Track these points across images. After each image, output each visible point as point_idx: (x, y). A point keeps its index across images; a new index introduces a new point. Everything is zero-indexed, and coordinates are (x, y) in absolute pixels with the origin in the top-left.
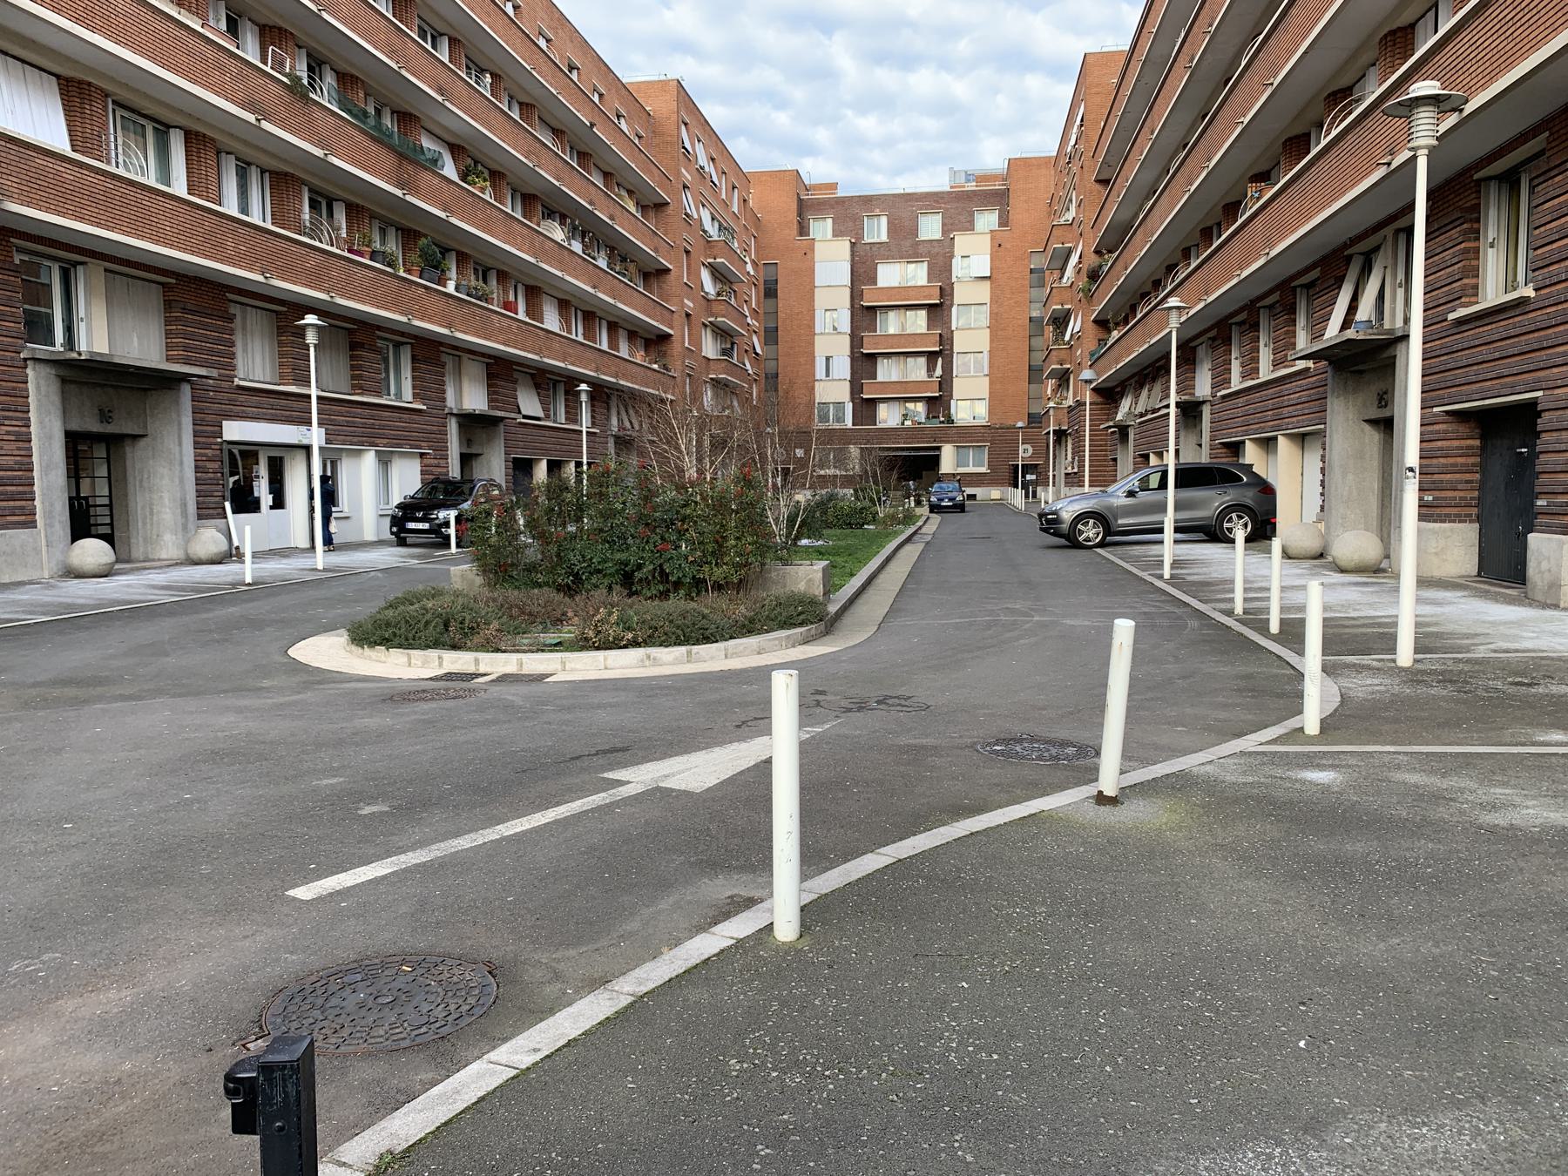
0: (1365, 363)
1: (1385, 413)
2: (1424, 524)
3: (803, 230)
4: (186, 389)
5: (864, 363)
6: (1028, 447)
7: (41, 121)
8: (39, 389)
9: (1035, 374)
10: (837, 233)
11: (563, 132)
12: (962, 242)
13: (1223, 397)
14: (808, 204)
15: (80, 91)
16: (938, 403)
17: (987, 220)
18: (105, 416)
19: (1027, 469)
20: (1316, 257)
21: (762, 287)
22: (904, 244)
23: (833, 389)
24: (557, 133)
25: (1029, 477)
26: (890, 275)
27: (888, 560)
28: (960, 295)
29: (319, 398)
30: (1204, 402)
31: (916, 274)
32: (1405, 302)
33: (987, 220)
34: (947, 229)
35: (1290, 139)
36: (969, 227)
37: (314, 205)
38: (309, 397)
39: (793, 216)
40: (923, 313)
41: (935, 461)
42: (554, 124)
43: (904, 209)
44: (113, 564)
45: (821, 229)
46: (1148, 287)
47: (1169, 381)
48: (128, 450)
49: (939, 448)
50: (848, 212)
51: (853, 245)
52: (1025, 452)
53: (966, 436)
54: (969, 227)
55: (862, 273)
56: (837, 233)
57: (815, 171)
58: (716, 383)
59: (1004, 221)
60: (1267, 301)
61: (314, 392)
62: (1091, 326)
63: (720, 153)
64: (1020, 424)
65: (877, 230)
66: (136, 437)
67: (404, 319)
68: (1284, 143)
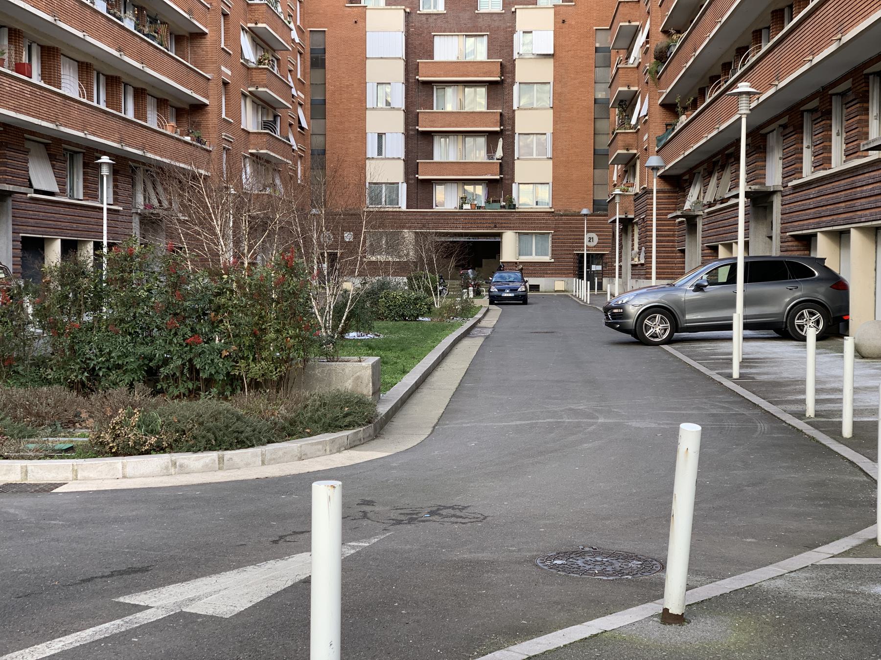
5: (419, 141)
6: (593, 235)
9: (600, 158)
13: (795, 187)
19: (592, 259)
21: (308, 57)
23: (386, 168)
29: (108, 209)
30: (774, 192)
31: (477, 49)
38: (102, 209)
40: (482, 91)
46: (718, 70)
47: (738, 169)
51: (408, 15)
53: (529, 223)
55: (417, 45)
58: (257, 159)
64: (585, 211)
68: (773, 12)
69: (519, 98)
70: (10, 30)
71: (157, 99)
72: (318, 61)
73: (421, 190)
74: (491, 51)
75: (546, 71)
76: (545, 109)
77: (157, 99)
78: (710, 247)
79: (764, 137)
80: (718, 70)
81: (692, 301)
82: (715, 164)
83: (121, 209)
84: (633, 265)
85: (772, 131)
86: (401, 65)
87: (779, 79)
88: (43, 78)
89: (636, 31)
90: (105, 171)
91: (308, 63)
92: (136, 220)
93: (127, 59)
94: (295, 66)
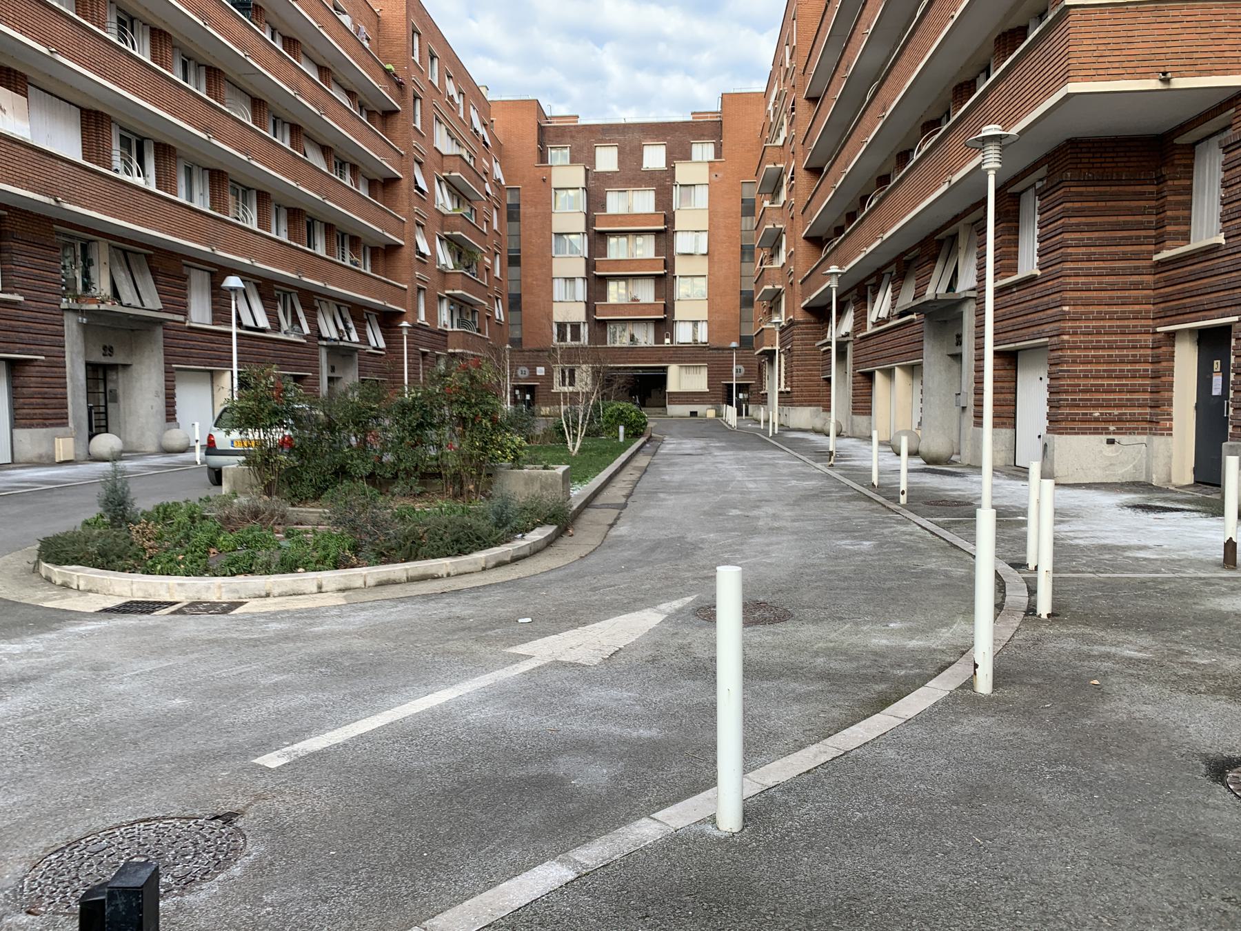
0: (944, 317)
1: (957, 350)
2: (998, 430)
3: (543, 157)
4: (159, 332)
5: (597, 283)
6: (741, 367)
7: (65, 142)
8: (71, 328)
9: (747, 300)
10: (573, 161)
11: (295, 41)
12: (683, 173)
13: (862, 338)
14: (548, 134)
15: (94, 122)
16: (664, 325)
17: (703, 151)
18: (108, 350)
19: (741, 388)
20: (894, 256)
21: (505, 212)
22: (632, 175)
23: (568, 304)
24: (350, 94)
25: (741, 396)
26: (616, 203)
27: (616, 473)
28: (680, 267)
29: (238, 335)
30: (966, 299)
31: (643, 202)
32: (976, 274)
33: (703, 151)
34: (671, 159)
35: (1004, 34)
36: (687, 156)
37: (125, 143)
38: (231, 334)
39: (534, 145)
40: (651, 240)
41: (662, 380)
42: (348, 86)
43: (629, 138)
44: (122, 452)
45: (558, 155)
46: (843, 221)
47: (983, 243)
48: (120, 375)
49: (665, 369)
50: (582, 140)
51: (587, 170)
52: (737, 374)
53: (690, 355)
54: (687, 156)
55: (595, 201)
56: (573, 161)
57: (555, 109)
58: (453, 299)
59: (718, 154)
60: (889, 270)
61: (234, 330)
62: (802, 244)
63: (456, 70)
64: (734, 344)
65: (607, 159)
66: (126, 366)
67: (321, 284)
68: (898, 156)
69: (682, 289)
70: (288, 209)
71: (82, 109)
72: (513, 214)
73: (600, 327)
74: (658, 205)
75: (702, 266)
76: (694, 333)
77: (82, 109)
78: (863, 374)
79: (1016, 198)
80: (935, 115)
81: (703, 403)
82: (908, 264)
83: (21, 299)
84: (780, 393)
85: (1026, 190)
86: (583, 217)
87: (884, 233)
88: (158, 187)
89: (781, 173)
90: (405, 332)
91: (505, 218)
92: (323, 356)
93: (301, 188)
94: (491, 217)
